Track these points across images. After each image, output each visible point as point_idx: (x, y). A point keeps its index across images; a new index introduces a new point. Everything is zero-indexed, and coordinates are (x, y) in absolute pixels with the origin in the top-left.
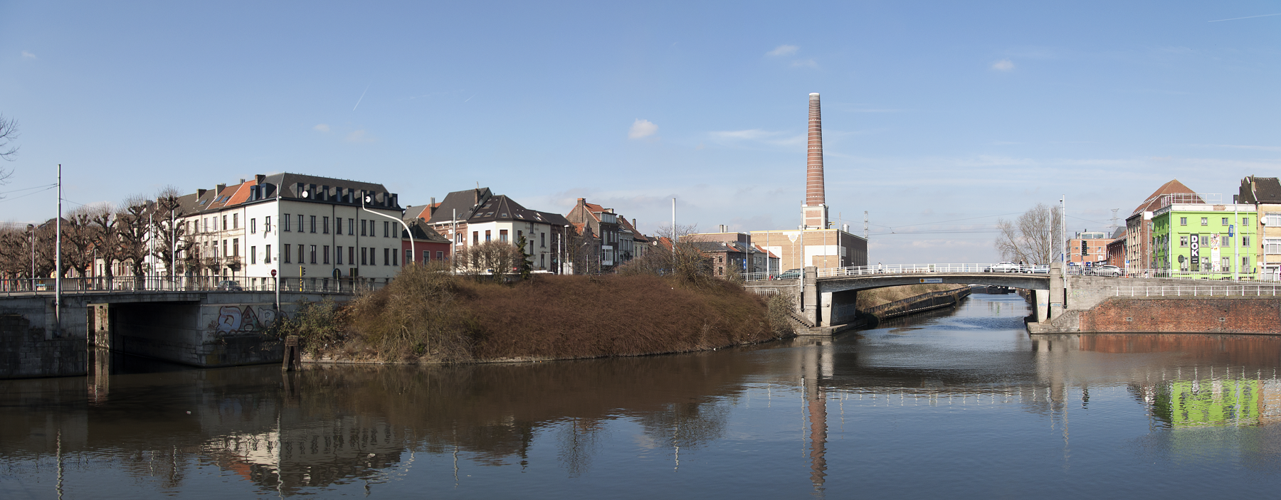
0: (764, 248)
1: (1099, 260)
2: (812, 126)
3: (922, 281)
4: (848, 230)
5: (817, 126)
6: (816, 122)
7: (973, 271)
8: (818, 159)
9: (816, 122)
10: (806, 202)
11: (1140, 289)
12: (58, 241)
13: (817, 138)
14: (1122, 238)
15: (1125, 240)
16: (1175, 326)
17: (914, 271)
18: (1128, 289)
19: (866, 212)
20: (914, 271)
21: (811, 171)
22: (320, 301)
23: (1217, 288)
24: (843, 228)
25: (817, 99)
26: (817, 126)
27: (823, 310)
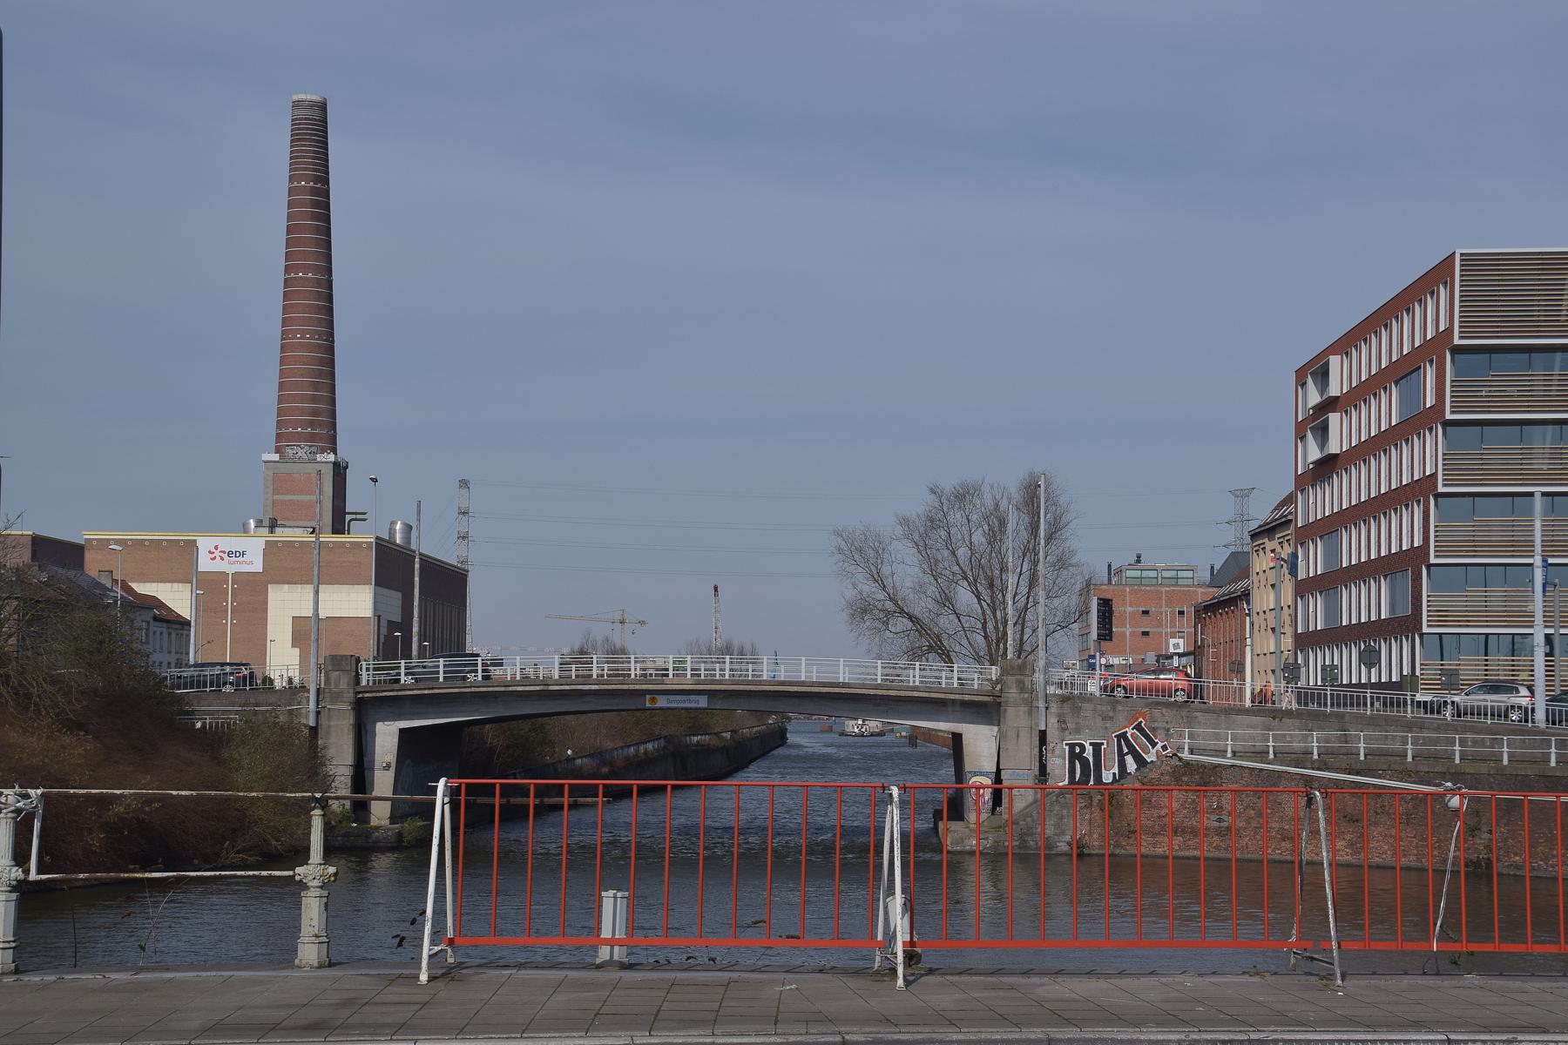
0: (142, 588)
1: (1172, 650)
2: (301, 204)
3: (653, 700)
4: (407, 538)
5: (315, 204)
6: (314, 191)
7: (792, 677)
8: (318, 309)
9: (314, 191)
10: (273, 445)
11: (1252, 738)
12: (803, 867)
13: (317, 243)
14: (1241, 585)
15: (1246, 595)
16: (1351, 844)
17: (513, 677)
18: (1217, 737)
19: (464, 484)
20: (513, 677)
21: (294, 347)
22: (1322, 432)
23: (1475, 742)
24: (392, 532)
25: (316, 114)
26: (315, 204)
27: (895, 842)
